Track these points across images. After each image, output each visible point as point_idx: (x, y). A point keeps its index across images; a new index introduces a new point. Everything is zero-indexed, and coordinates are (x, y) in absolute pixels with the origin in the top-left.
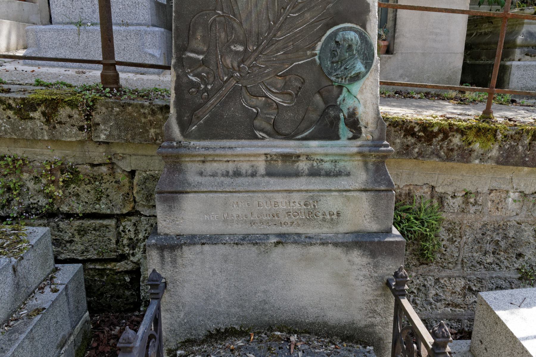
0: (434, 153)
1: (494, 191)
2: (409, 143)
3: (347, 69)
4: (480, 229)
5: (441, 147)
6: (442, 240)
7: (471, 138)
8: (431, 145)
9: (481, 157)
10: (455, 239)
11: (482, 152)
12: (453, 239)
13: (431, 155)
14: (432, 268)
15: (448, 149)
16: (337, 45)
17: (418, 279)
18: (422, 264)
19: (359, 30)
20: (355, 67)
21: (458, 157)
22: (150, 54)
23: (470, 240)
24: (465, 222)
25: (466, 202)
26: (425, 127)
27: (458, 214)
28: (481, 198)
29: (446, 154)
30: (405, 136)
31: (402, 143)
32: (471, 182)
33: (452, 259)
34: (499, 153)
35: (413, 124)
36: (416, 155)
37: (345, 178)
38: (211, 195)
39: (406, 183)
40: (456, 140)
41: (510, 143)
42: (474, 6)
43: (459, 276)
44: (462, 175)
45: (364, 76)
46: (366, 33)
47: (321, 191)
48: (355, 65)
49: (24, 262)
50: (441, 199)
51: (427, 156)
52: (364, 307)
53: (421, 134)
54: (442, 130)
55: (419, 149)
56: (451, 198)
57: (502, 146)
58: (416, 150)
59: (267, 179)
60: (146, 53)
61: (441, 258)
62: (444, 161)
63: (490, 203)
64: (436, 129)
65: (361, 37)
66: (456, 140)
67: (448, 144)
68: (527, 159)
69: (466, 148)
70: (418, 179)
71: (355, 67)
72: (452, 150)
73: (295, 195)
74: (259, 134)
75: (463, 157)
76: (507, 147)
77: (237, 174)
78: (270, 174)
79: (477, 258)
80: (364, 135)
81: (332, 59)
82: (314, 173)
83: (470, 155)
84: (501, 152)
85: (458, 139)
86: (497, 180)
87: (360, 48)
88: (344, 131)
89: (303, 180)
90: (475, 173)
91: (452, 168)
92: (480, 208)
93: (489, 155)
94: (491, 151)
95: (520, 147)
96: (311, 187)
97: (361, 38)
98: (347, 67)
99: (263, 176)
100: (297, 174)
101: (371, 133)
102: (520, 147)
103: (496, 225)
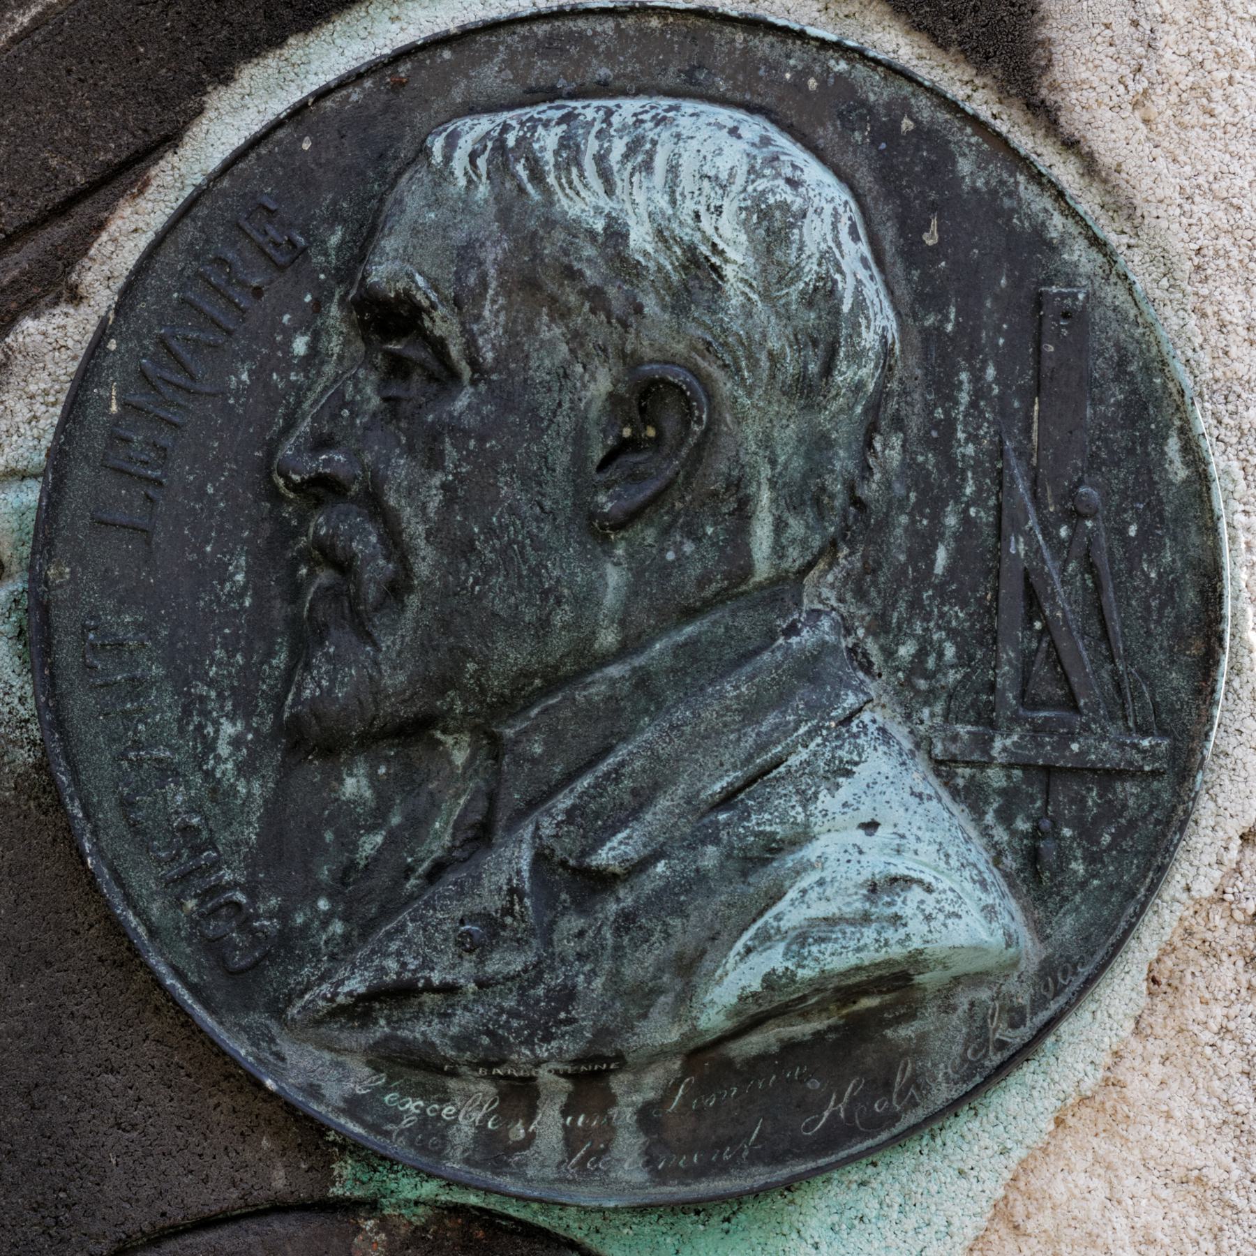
3: (604, 881)
16: (398, 368)
19: (876, 90)
20: (773, 848)
46: (1024, 140)
48: (764, 822)
52: (1202, 811)
65: (910, 227)
71: (773, 848)
81: (300, 658)
87: (891, 451)
97: (913, 253)
98: (606, 856)
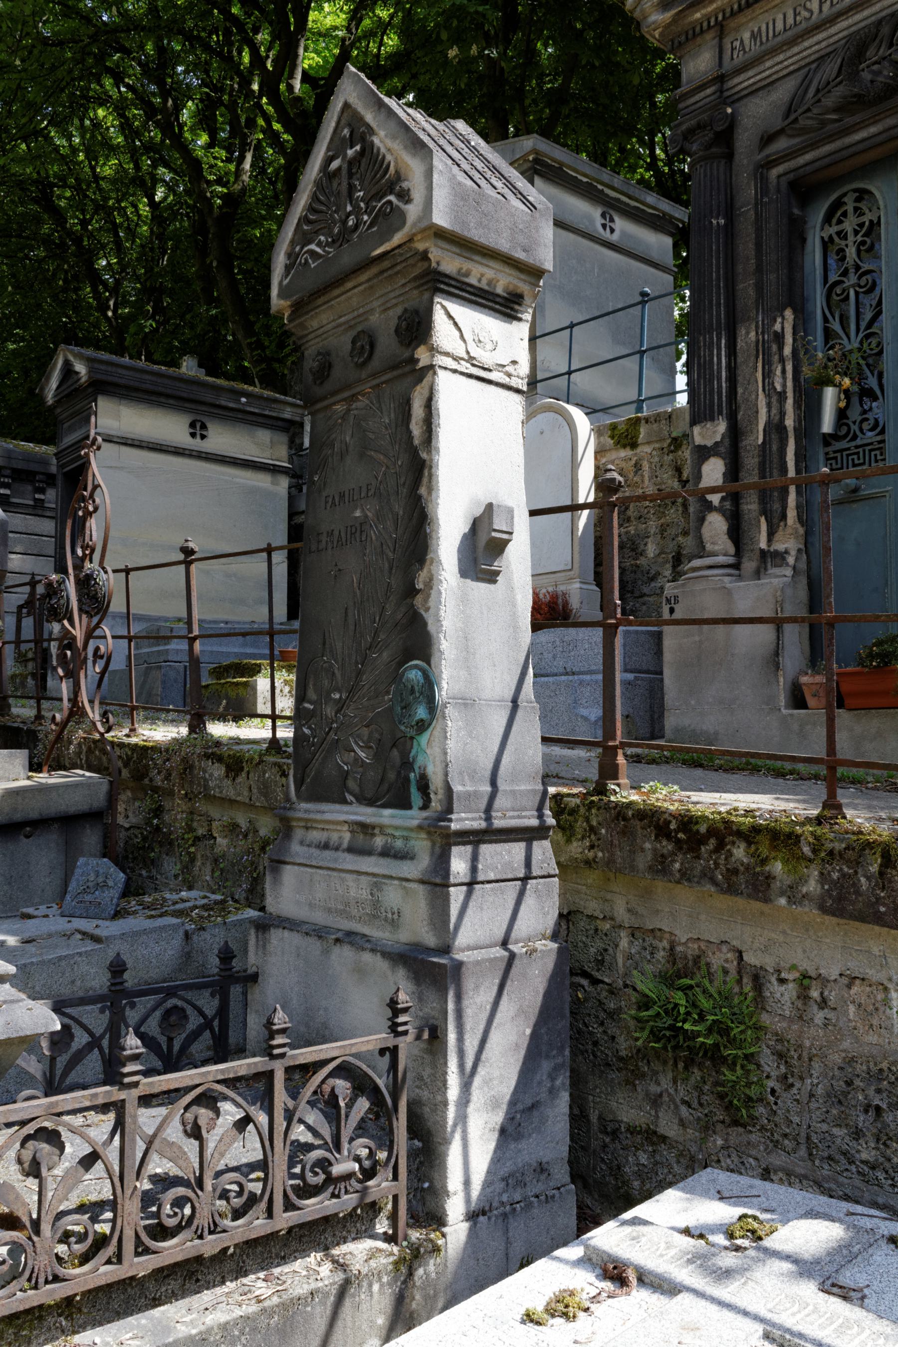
0: (705, 875)
1: (858, 982)
2: (665, 851)
4: (841, 1068)
5: (717, 864)
6: (768, 1077)
7: (764, 851)
8: (698, 857)
9: (789, 893)
10: (791, 1080)
11: (788, 883)
12: (786, 1078)
13: (701, 877)
14: (754, 1138)
15: (728, 870)
17: (729, 1156)
18: (736, 1123)
21: (747, 887)
22: (582, 716)
23: (820, 1090)
24: (807, 1043)
25: (803, 995)
26: (687, 821)
27: (791, 1020)
28: (833, 993)
29: (727, 879)
30: (657, 837)
31: (655, 850)
32: (804, 951)
33: (788, 1127)
34: (823, 887)
35: (666, 816)
36: (678, 875)
37: (409, 862)
38: (302, 869)
39: (690, 935)
40: (740, 852)
41: (841, 870)
42: (242, 650)
43: (806, 1177)
44: (784, 932)
45: (430, 725)
47: (385, 876)
49: (206, 935)
50: (758, 979)
51: (696, 879)
53: (681, 835)
54: (713, 831)
55: (682, 864)
56: (775, 983)
57: (825, 872)
58: (677, 866)
59: (346, 855)
60: (577, 715)
61: (769, 1121)
62: (723, 891)
63: (852, 1009)
64: (703, 829)
66: (740, 852)
67: (726, 859)
68: (882, 909)
69: (758, 869)
70: (710, 930)
72: (735, 872)
73: (363, 877)
74: (349, 797)
75: (756, 889)
76: (835, 876)
77: (326, 846)
78: (351, 850)
79: (838, 1141)
80: (433, 804)
82: (387, 853)
83: (769, 885)
84: (826, 887)
85: (742, 850)
86: (853, 952)
88: (416, 798)
89: (372, 859)
90: (807, 930)
91: (762, 913)
92: (831, 1015)
93: (804, 890)
94: (806, 881)
95: (863, 880)
96: (376, 870)
99: (344, 851)
100: (366, 852)
101: (440, 801)
102: (863, 880)
103: (874, 1069)
